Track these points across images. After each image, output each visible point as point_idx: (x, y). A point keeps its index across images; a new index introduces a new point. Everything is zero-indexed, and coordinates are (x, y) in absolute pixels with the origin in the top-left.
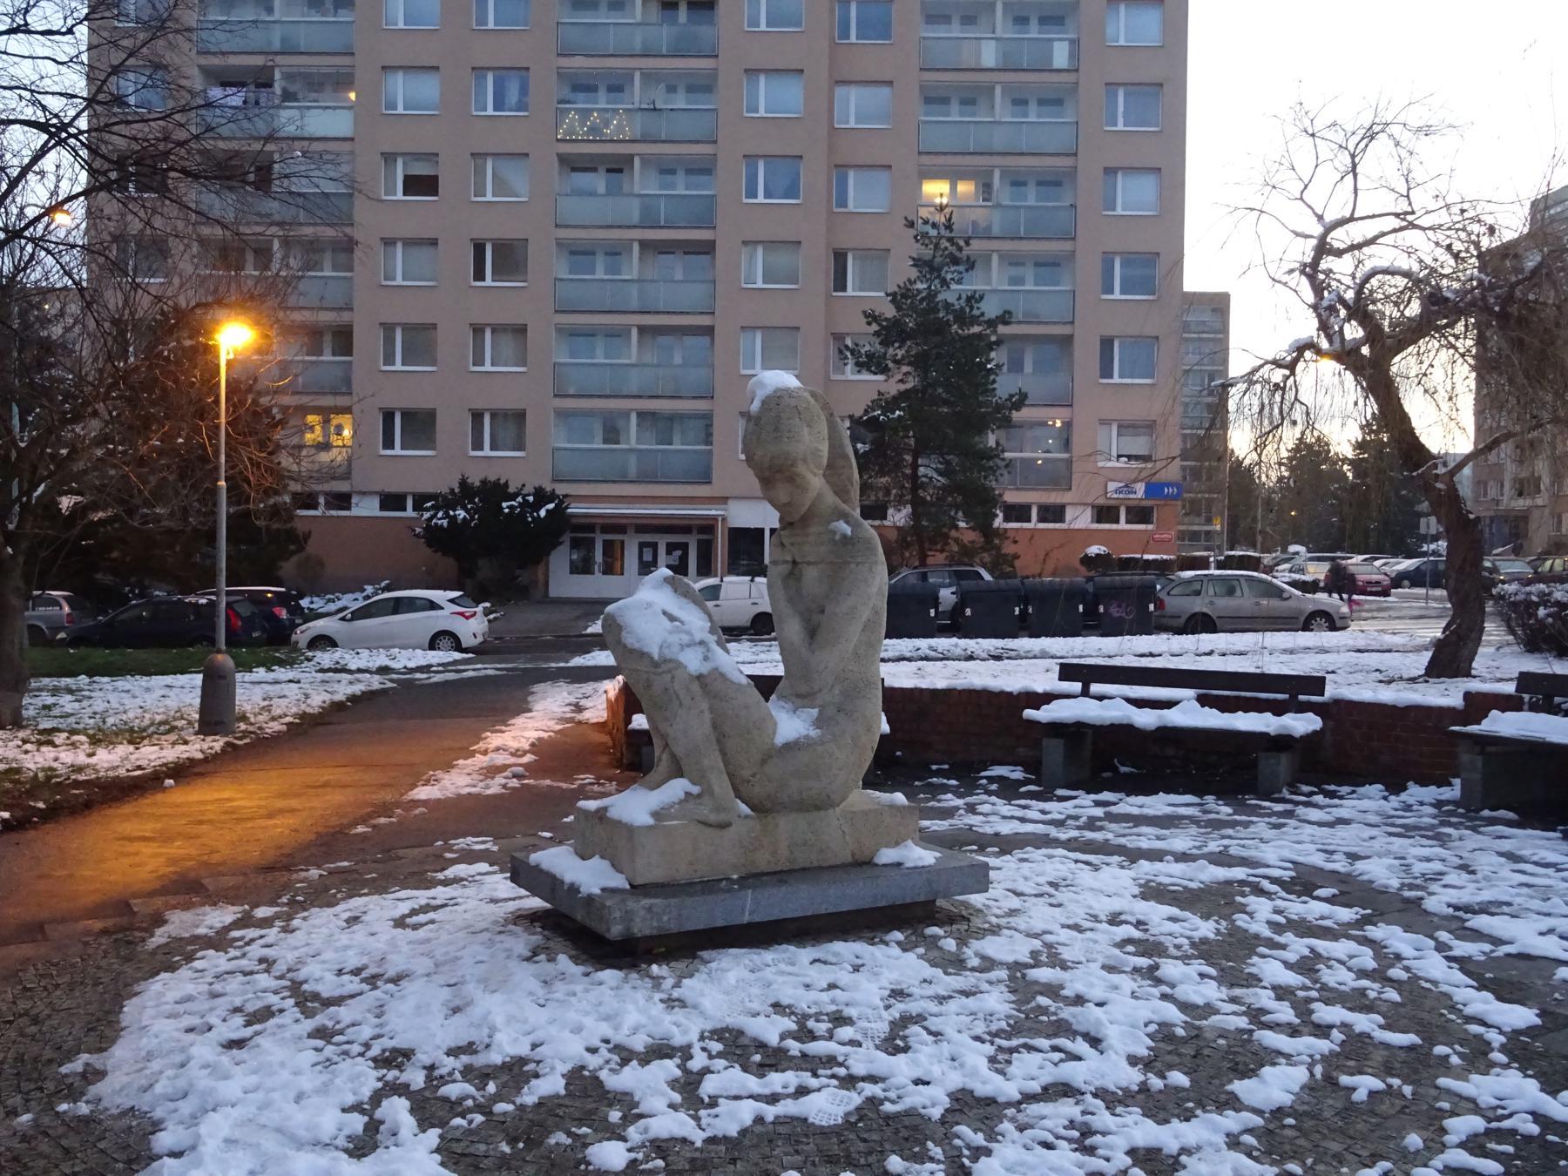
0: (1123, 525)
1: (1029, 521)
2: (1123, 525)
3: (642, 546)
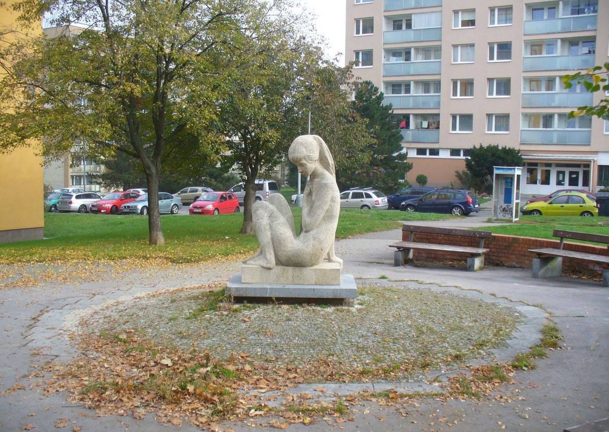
0: (428, 156)
1: (459, 155)
2: (428, 156)
3: (559, 173)
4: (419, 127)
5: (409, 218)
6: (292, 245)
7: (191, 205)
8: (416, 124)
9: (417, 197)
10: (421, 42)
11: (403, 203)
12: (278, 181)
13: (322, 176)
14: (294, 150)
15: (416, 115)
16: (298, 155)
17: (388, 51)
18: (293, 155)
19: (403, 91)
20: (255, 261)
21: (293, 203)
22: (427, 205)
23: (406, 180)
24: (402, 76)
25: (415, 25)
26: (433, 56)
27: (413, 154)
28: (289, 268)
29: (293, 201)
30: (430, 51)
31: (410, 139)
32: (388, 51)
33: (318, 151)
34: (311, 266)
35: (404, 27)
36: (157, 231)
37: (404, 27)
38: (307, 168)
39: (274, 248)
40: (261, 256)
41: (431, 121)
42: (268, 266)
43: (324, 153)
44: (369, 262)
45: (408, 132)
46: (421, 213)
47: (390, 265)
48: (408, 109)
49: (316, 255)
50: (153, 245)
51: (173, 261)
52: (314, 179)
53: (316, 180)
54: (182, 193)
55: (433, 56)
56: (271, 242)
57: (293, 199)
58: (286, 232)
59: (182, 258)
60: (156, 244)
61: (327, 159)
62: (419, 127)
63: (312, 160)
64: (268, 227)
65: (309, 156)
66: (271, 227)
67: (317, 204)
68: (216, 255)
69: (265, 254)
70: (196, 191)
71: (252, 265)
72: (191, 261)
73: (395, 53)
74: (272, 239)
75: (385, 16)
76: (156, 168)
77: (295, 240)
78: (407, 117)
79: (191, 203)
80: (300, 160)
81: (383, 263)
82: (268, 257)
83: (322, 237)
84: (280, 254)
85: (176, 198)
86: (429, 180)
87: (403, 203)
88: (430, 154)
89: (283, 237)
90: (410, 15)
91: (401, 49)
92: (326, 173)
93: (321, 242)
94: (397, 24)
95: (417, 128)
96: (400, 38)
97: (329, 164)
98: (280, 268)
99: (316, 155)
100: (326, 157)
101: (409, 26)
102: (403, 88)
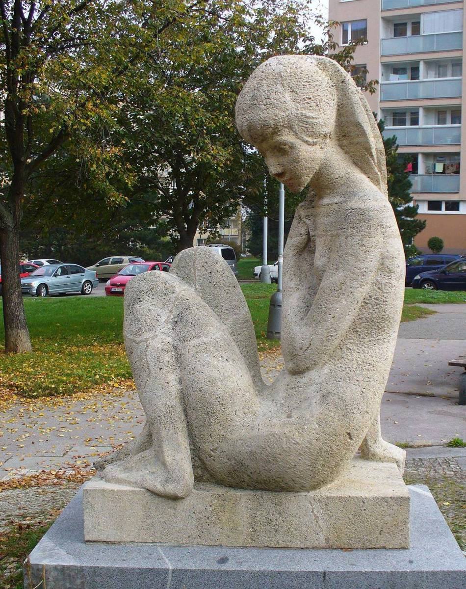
0: (443, 211)
2: (443, 211)
4: (431, 171)
5: (431, 300)
6: (248, 419)
7: (109, 282)
8: (427, 167)
9: (438, 268)
10: (434, 52)
11: (418, 277)
12: (236, 248)
13: (349, 190)
14: (254, 97)
15: (426, 155)
16: (265, 115)
17: (386, 66)
18: (249, 116)
19: (408, 121)
20: (127, 469)
21: (257, 277)
22: (450, 280)
23: (413, 245)
24: (407, 100)
25: (425, 29)
26: (450, 71)
27: (423, 209)
28: (239, 493)
29: (256, 275)
30: (446, 66)
31: (419, 189)
32: (386, 66)
33: (334, 104)
34: (314, 488)
35: (409, 33)
36: (17, 327)
37: (409, 33)
38: (296, 160)
39: (189, 425)
40: (147, 454)
41: (447, 162)
42: (170, 489)
43: (353, 114)
44: (409, 394)
45: (416, 178)
46: (447, 292)
47: (448, 398)
48: (416, 146)
49: (330, 453)
50: (11, 355)
51: (22, 394)
52: (321, 198)
53: (326, 201)
54: (101, 264)
55: (450, 71)
56: (179, 409)
57: (256, 272)
58: (226, 371)
59: (40, 387)
60: (15, 350)
61: (363, 133)
62: (431, 172)
63: (313, 134)
64: (168, 358)
65: (304, 121)
66: (179, 358)
67: (331, 279)
68: (109, 378)
69: (160, 447)
70: (121, 262)
71: (119, 481)
72: (57, 391)
73: (396, 69)
74: (183, 397)
75: (383, 18)
76: (14, 217)
77: (257, 400)
78: (414, 157)
79: (109, 279)
80: (276, 131)
81: (432, 396)
82: (168, 459)
83: (350, 390)
84: (207, 447)
85: (90, 272)
86: (446, 245)
87: (418, 277)
88: (447, 209)
89: (220, 392)
90: (419, 15)
91: (405, 63)
92: (358, 176)
93: (346, 412)
94: (399, 27)
95: (428, 173)
96: (402, 48)
97: (368, 149)
98: (211, 494)
99: (326, 118)
100: (358, 125)
101: (416, 30)
102: (408, 119)
